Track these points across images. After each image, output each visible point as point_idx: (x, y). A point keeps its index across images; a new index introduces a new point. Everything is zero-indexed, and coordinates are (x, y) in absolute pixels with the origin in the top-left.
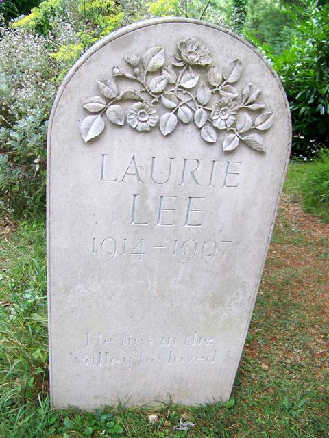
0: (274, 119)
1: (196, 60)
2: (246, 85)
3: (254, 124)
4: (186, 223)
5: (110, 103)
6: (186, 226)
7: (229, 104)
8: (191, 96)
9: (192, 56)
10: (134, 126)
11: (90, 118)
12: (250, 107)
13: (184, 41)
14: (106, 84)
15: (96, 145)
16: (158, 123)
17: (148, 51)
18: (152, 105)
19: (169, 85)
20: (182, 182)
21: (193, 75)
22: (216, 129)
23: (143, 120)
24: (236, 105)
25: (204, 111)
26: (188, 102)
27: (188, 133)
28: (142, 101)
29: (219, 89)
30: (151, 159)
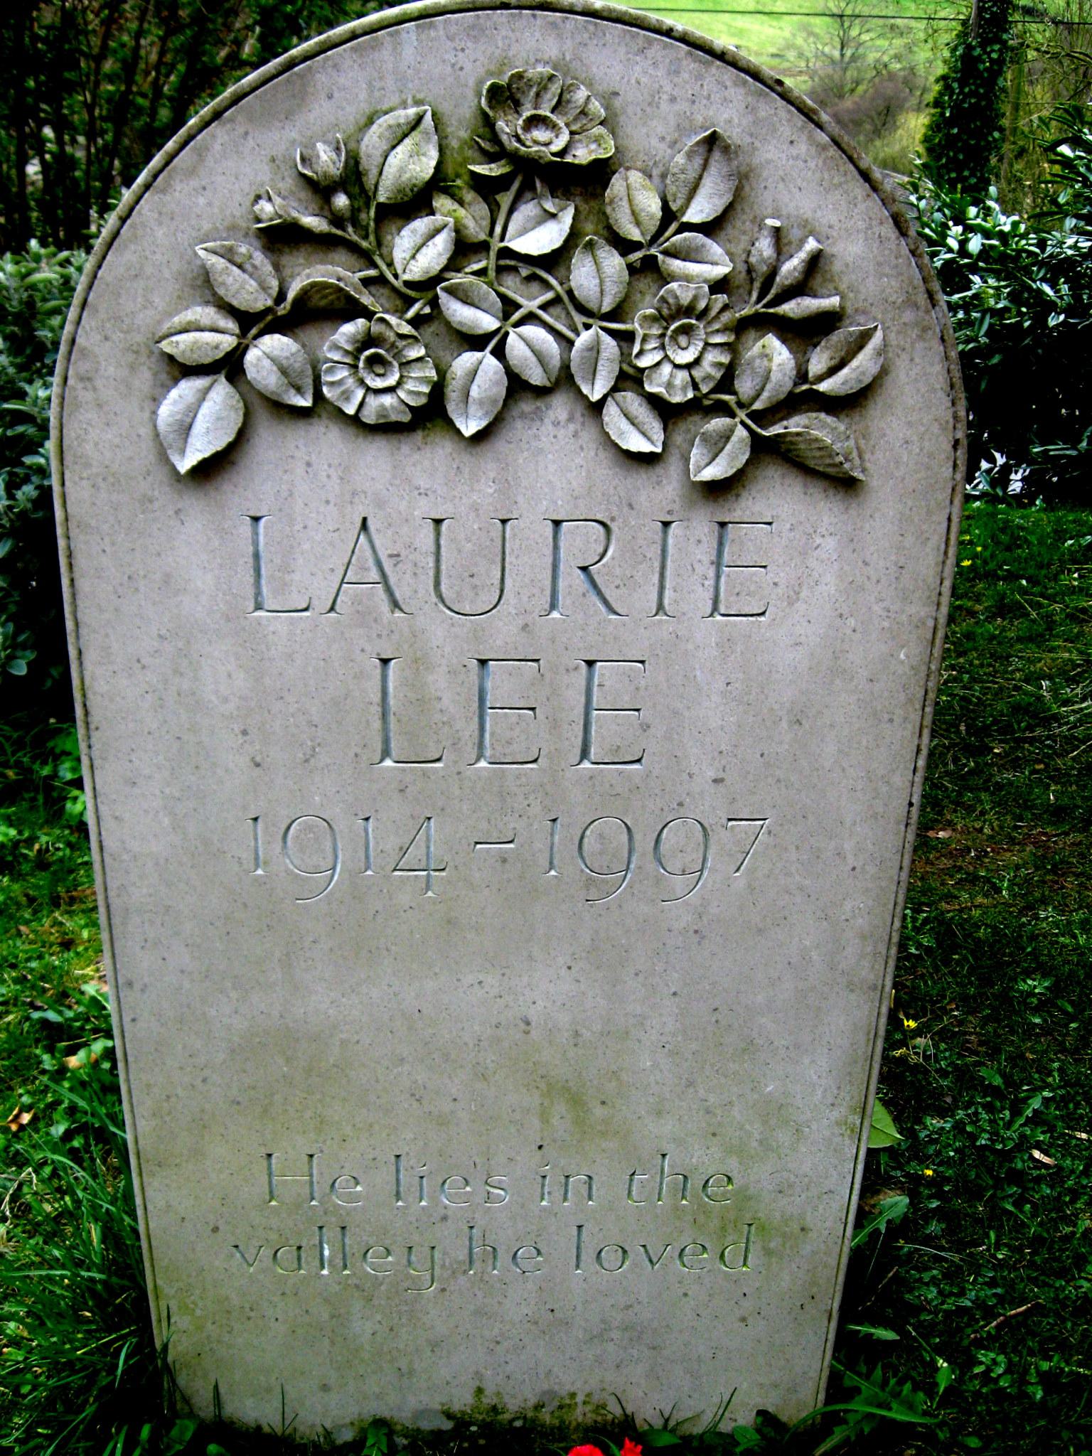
0: (882, 351)
1: (555, 148)
2: (761, 226)
3: (802, 376)
4: (585, 754)
5: (254, 331)
6: (586, 765)
7: (702, 305)
8: (548, 286)
9: (540, 134)
10: (350, 410)
11: (188, 388)
12: (791, 308)
13: (503, 80)
14: (231, 261)
15: (227, 487)
16: (438, 391)
17: (374, 127)
18: (406, 329)
19: (464, 249)
20: (553, 606)
21: (549, 206)
22: (655, 402)
23: (379, 383)
24: (725, 308)
25: (608, 340)
26: (543, 307)
27: (556, 424)
28: (368, 315)
29: (653, 251)
30: (431, 525)
